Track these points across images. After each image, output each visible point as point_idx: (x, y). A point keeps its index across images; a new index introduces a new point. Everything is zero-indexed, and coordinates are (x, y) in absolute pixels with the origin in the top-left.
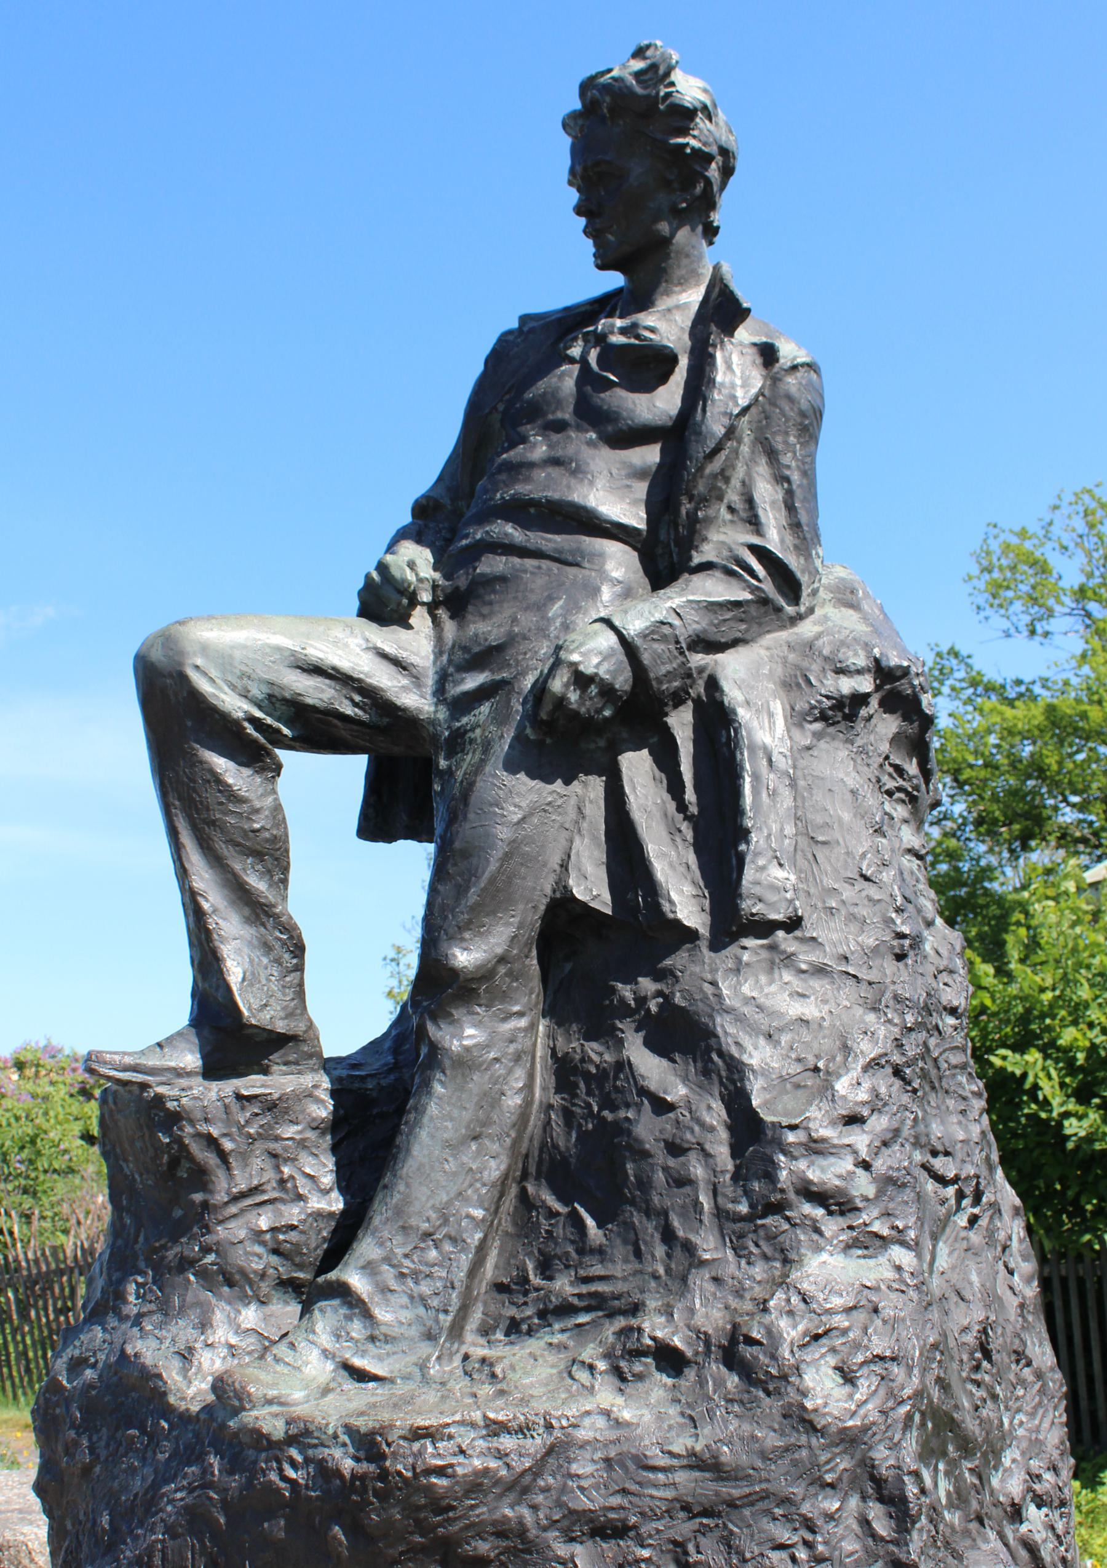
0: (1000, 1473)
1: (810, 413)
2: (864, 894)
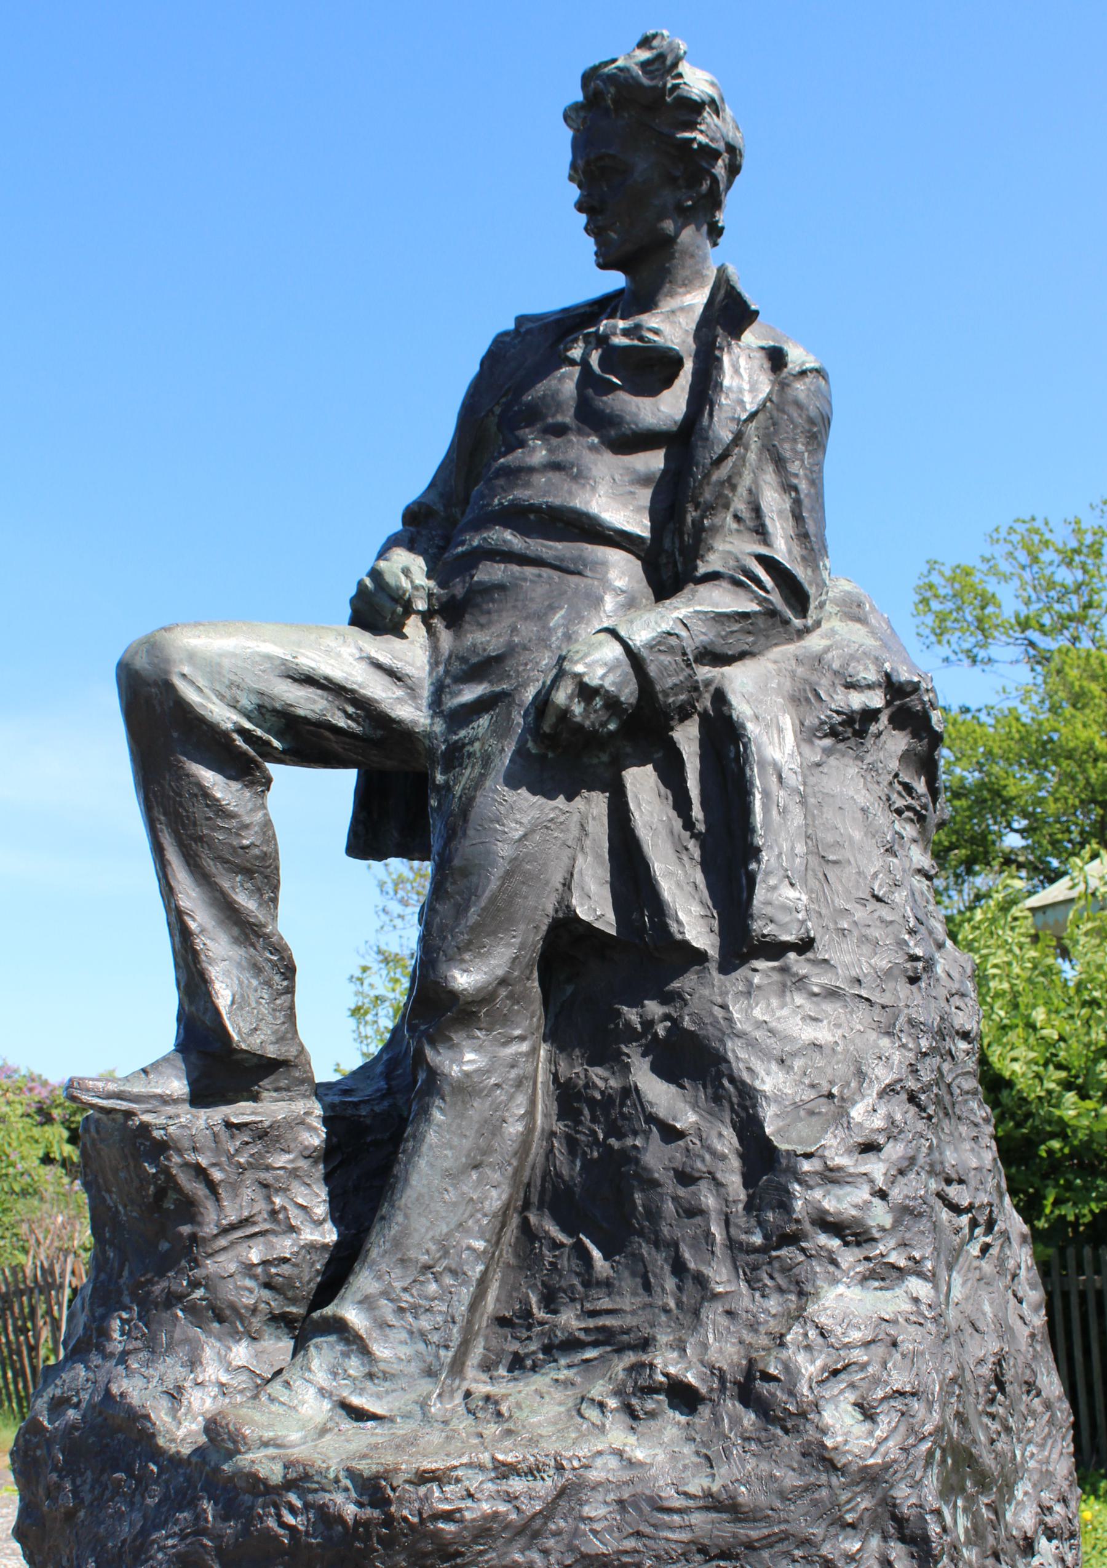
0: (1013, 1507)
1: (819, 420)
2: (876, 914)
